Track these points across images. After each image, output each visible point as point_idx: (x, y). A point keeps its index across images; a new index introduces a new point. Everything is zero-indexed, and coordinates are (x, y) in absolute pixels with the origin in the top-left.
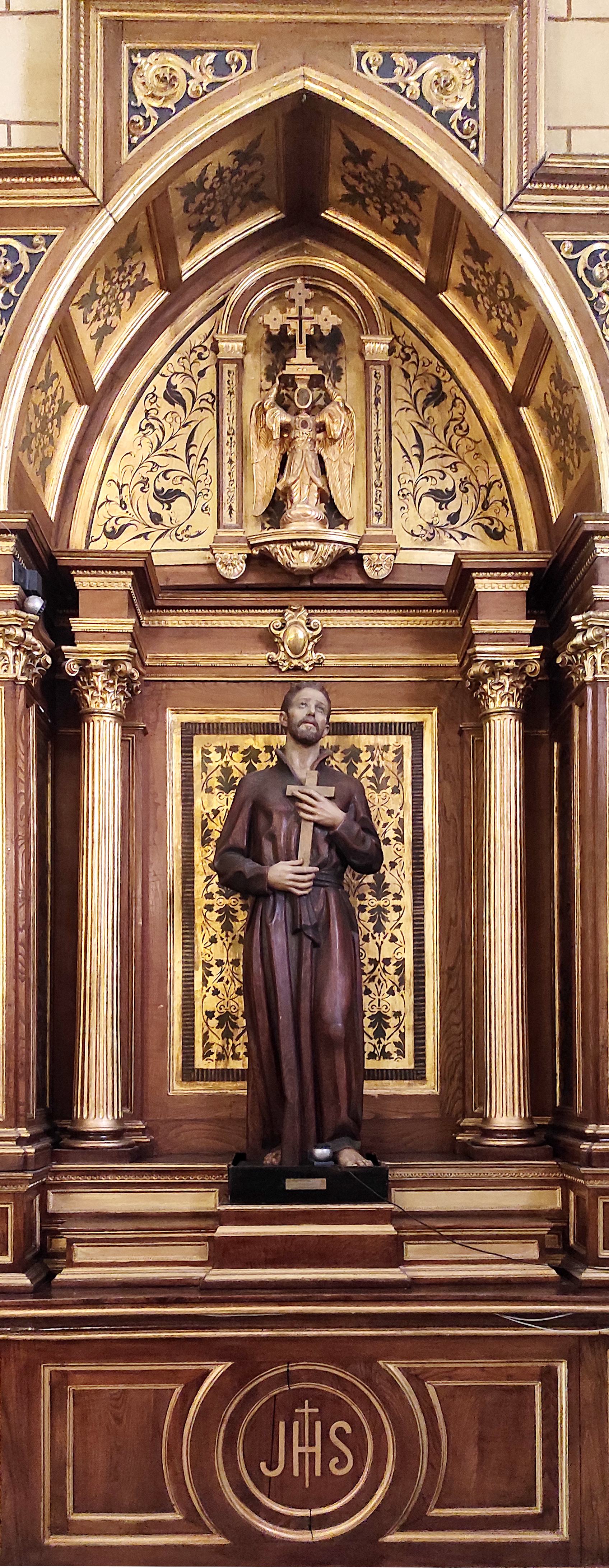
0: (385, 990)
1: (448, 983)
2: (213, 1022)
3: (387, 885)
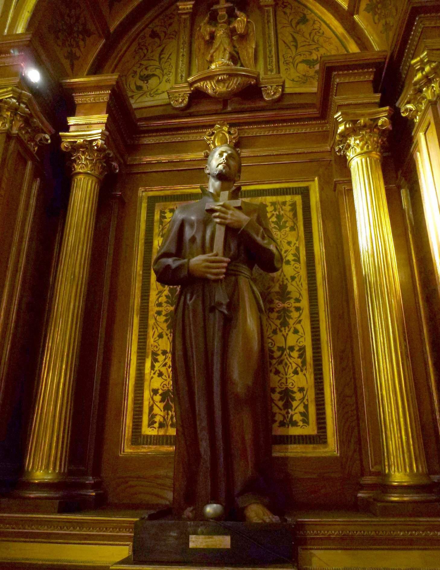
0: (291, 371)
1: (341, 363)
2: (158, 398)
3: (289, 293)
